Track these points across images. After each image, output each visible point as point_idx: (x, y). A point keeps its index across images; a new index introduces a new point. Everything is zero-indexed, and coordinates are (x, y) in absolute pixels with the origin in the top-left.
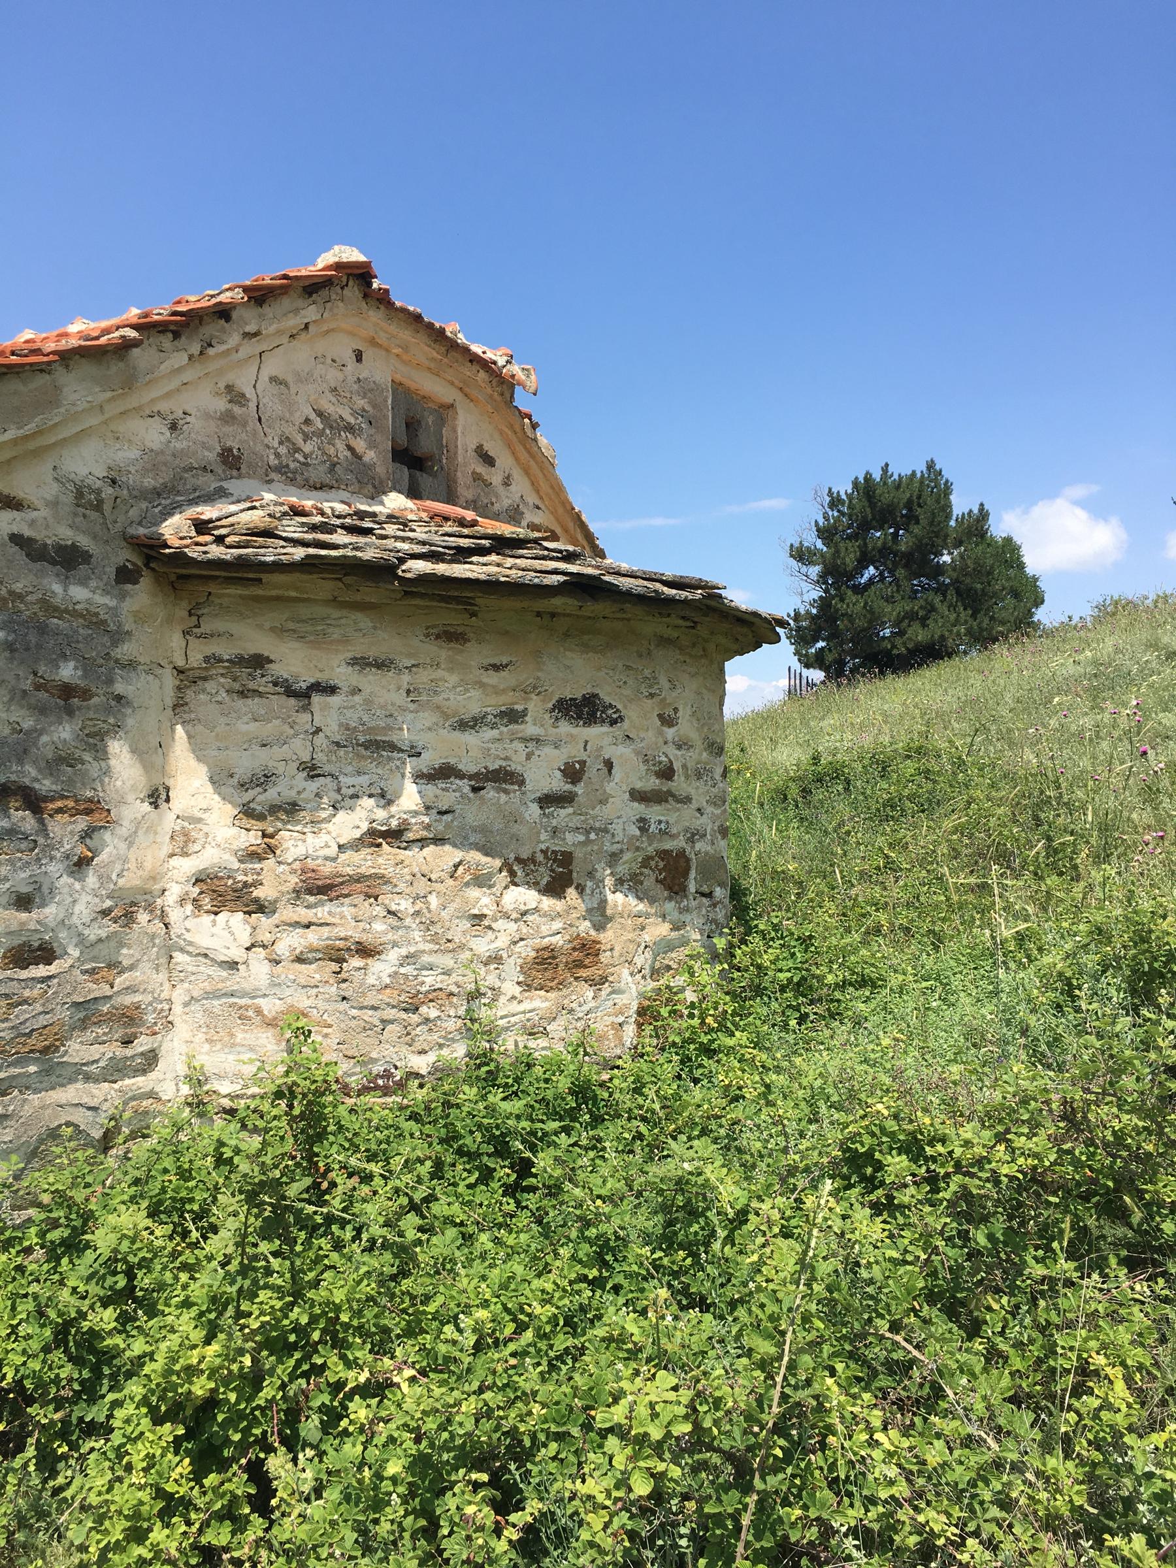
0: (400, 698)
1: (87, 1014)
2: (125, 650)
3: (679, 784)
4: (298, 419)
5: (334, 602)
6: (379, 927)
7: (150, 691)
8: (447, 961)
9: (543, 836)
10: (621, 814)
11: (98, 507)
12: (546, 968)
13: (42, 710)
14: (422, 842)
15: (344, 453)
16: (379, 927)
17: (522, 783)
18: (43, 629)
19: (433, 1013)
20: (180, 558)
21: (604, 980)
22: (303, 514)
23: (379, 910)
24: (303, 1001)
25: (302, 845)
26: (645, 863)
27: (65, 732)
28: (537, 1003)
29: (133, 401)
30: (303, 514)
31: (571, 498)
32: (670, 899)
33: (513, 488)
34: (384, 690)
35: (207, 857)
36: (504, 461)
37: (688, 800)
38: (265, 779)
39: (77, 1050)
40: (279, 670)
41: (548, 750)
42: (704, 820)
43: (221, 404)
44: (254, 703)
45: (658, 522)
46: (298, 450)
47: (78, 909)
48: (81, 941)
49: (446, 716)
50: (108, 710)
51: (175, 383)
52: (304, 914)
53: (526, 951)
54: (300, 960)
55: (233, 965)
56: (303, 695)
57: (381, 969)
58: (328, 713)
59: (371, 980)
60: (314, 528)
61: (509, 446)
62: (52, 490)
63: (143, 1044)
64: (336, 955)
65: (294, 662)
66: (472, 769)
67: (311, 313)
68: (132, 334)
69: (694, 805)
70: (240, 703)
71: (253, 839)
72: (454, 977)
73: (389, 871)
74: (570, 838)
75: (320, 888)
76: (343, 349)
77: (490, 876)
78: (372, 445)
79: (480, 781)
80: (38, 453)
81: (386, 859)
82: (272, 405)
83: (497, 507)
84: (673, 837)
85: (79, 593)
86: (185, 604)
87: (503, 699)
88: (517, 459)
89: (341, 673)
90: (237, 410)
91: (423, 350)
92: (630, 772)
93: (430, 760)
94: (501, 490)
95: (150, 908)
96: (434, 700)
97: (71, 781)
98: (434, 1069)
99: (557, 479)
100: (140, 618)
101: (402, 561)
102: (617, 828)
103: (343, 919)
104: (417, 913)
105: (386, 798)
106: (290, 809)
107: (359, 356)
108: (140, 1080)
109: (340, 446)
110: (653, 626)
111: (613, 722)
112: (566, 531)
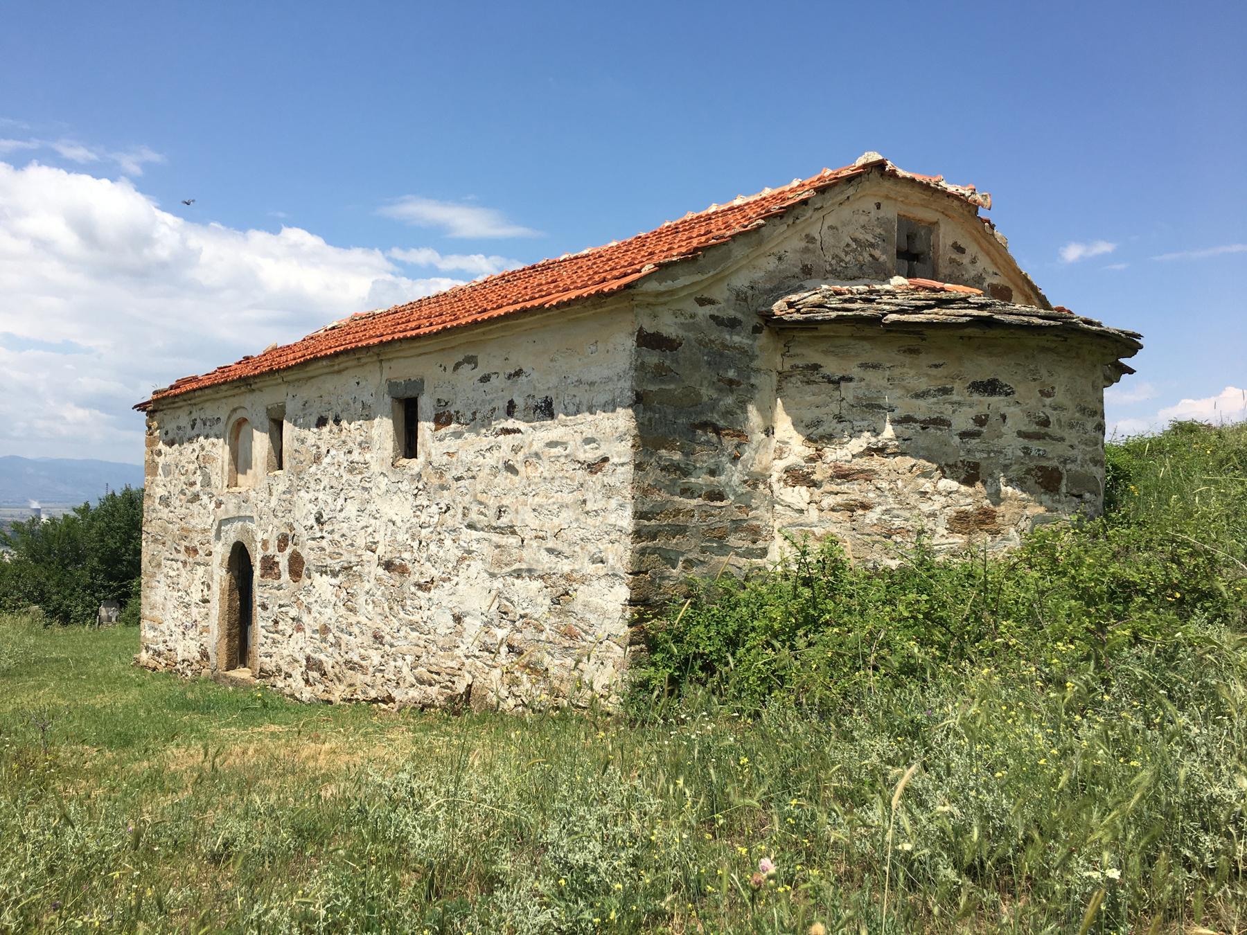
0: (885, 383)
1: (737, 526)
2: (755, 364)
3: (1053, 429)
4: (843, 244)
5: (852, 336)
6: (871, 495)
7: (766, 382)
8: (907, 514)
9: (962, 453)
10: (1012, 445)
11: (746, 300)
12: (961, 522)
13: (720, 390)
14: (895, 454)
15: (867, 258)
16: (871, 495)
17: (950, 425)
18: (721, 355)
19: (899, 540)
20: (780, 320)
21: (998, 532)
22: (841, 294)
23: (871, 487)
24: (834, 530)
25: (836, 454)
26: (1028, 472)
27: (729, 400)
28: (957, 540)
29: (762, 250)
30: (841, 294)
31: (1019, 266)
32: (1045, 493)
33: (978, 264)
34: (876, 379)
35: (791, 460)
36: (972, 249)
37: (1062, 439)
38: (818, 423)
39: (733, 540)
40: (825, 371)
41: (965, 409)
42: (1075, 452)
43: (803, 244)
44: (813, 387)
45: (1236, 248)
46: (842, 261)
47: (734, 478)
48: (735, 493)
49: (908, 391)
50: (748, 391)
51: (781, 238)
52: (835, 488)
53: (951, 512)
54: (833, 510)
55: (801, 511)
56: (836, 382)
57: (872, 516)
58: (849, 391)
59: (867, 521)
60: (845, 301)
61: (975, 240)
62: (727, 294)
63: (761, 544)
64: (850, 508)
65: (832, 367)
66: (922, 418)
67: (850, 191)
68: (761, 222)
69: (1067, 443)
70: (807, 387)
71: (811, 451)
72: (910, 522)
73: (877, 468)
74: (978, 455)
75: (843, 475)
76: (870, 205)
77: (931, 472)
78: (884, 252)
79: (926, 424)
80: (722, 279)
81: (875, 462)
82: (829, 240)
83: (966, 276)
84: (1049, 459)
85: (736, 339)
86: (783, 342)
87: (939, 382)
88: (981, 247)
89: (855, 371)
90: (811, 246)
91: (916, 195)
92: (1017, 419)
93: (899, 413)
94: (970, 267)
95: (765, 482)
96: (903, 384)
97: (731, 422)
98: (900, 568)
99: (1008, 256)
100: (762, 349)
101: (885, 315)
102: (1009, 451)
103: (854, 491)
104: (891, 489)
105: (876, 432)
106: (829, 438)
107: (878, 206)
108: (759, 561)
109: (866, 255)
110: (1033, 341)
111: (1007, 394)
112: (1017, 286)
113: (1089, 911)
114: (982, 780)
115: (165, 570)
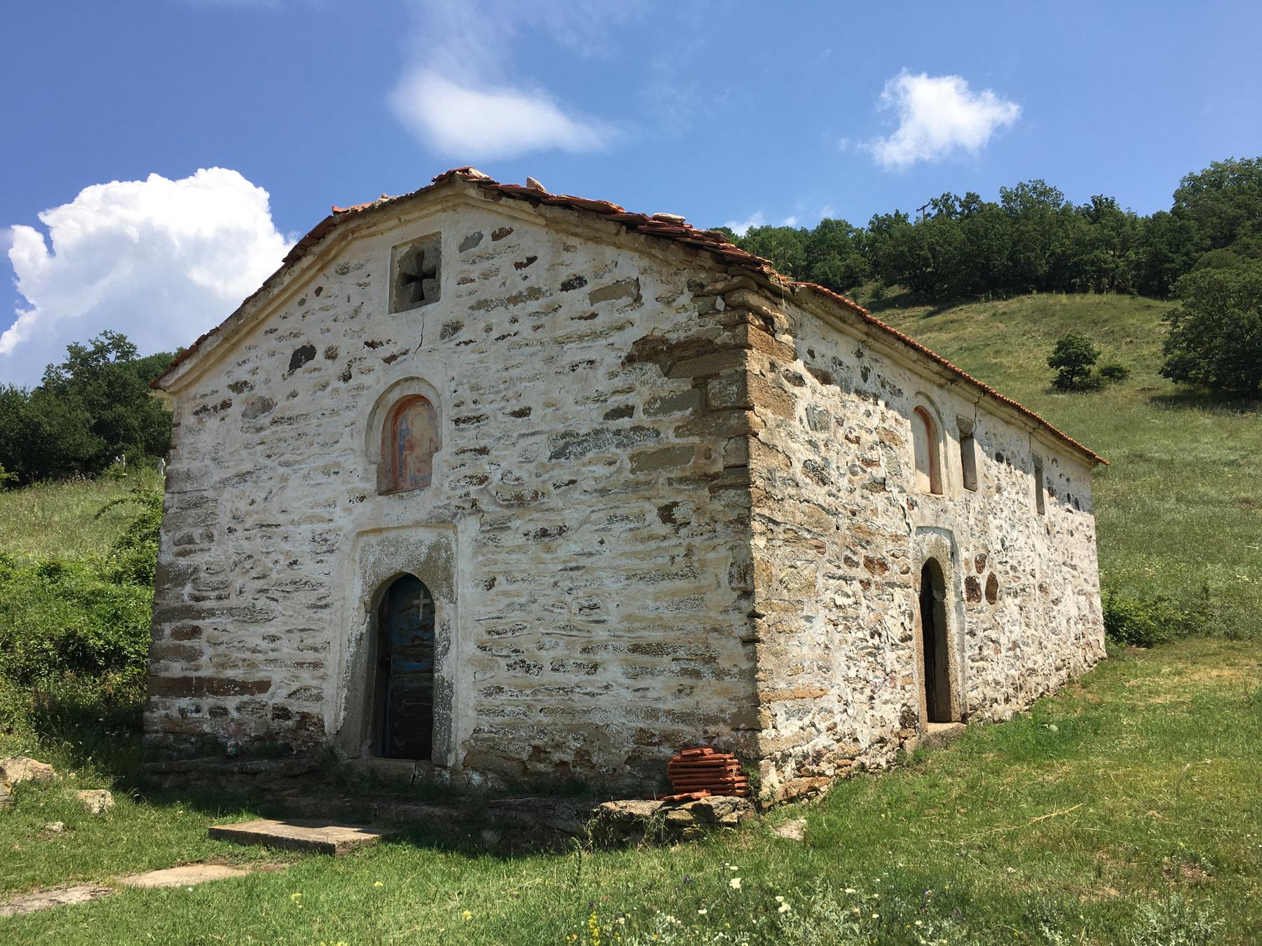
113: (960, 682)
114: (492, 397)
115: (827, 597)
